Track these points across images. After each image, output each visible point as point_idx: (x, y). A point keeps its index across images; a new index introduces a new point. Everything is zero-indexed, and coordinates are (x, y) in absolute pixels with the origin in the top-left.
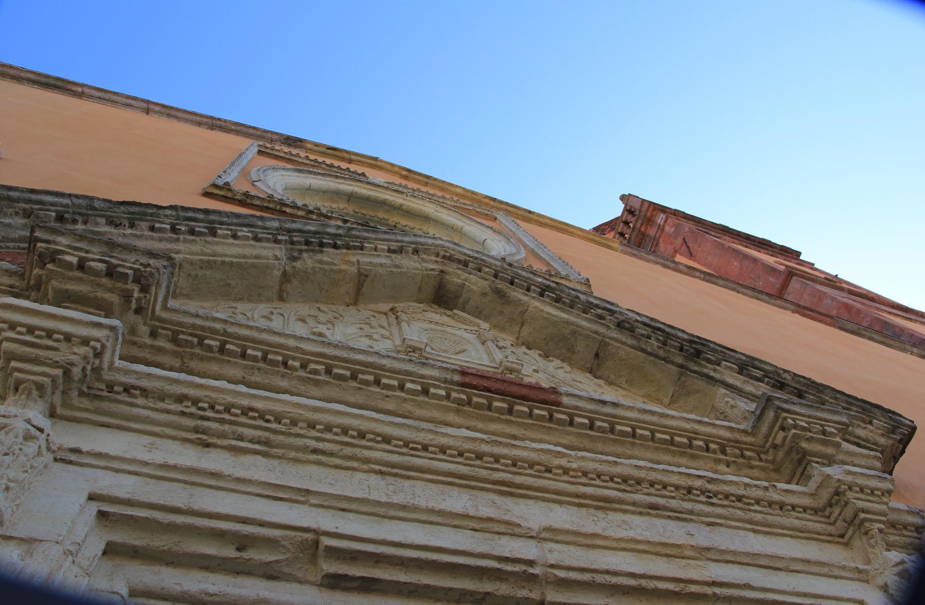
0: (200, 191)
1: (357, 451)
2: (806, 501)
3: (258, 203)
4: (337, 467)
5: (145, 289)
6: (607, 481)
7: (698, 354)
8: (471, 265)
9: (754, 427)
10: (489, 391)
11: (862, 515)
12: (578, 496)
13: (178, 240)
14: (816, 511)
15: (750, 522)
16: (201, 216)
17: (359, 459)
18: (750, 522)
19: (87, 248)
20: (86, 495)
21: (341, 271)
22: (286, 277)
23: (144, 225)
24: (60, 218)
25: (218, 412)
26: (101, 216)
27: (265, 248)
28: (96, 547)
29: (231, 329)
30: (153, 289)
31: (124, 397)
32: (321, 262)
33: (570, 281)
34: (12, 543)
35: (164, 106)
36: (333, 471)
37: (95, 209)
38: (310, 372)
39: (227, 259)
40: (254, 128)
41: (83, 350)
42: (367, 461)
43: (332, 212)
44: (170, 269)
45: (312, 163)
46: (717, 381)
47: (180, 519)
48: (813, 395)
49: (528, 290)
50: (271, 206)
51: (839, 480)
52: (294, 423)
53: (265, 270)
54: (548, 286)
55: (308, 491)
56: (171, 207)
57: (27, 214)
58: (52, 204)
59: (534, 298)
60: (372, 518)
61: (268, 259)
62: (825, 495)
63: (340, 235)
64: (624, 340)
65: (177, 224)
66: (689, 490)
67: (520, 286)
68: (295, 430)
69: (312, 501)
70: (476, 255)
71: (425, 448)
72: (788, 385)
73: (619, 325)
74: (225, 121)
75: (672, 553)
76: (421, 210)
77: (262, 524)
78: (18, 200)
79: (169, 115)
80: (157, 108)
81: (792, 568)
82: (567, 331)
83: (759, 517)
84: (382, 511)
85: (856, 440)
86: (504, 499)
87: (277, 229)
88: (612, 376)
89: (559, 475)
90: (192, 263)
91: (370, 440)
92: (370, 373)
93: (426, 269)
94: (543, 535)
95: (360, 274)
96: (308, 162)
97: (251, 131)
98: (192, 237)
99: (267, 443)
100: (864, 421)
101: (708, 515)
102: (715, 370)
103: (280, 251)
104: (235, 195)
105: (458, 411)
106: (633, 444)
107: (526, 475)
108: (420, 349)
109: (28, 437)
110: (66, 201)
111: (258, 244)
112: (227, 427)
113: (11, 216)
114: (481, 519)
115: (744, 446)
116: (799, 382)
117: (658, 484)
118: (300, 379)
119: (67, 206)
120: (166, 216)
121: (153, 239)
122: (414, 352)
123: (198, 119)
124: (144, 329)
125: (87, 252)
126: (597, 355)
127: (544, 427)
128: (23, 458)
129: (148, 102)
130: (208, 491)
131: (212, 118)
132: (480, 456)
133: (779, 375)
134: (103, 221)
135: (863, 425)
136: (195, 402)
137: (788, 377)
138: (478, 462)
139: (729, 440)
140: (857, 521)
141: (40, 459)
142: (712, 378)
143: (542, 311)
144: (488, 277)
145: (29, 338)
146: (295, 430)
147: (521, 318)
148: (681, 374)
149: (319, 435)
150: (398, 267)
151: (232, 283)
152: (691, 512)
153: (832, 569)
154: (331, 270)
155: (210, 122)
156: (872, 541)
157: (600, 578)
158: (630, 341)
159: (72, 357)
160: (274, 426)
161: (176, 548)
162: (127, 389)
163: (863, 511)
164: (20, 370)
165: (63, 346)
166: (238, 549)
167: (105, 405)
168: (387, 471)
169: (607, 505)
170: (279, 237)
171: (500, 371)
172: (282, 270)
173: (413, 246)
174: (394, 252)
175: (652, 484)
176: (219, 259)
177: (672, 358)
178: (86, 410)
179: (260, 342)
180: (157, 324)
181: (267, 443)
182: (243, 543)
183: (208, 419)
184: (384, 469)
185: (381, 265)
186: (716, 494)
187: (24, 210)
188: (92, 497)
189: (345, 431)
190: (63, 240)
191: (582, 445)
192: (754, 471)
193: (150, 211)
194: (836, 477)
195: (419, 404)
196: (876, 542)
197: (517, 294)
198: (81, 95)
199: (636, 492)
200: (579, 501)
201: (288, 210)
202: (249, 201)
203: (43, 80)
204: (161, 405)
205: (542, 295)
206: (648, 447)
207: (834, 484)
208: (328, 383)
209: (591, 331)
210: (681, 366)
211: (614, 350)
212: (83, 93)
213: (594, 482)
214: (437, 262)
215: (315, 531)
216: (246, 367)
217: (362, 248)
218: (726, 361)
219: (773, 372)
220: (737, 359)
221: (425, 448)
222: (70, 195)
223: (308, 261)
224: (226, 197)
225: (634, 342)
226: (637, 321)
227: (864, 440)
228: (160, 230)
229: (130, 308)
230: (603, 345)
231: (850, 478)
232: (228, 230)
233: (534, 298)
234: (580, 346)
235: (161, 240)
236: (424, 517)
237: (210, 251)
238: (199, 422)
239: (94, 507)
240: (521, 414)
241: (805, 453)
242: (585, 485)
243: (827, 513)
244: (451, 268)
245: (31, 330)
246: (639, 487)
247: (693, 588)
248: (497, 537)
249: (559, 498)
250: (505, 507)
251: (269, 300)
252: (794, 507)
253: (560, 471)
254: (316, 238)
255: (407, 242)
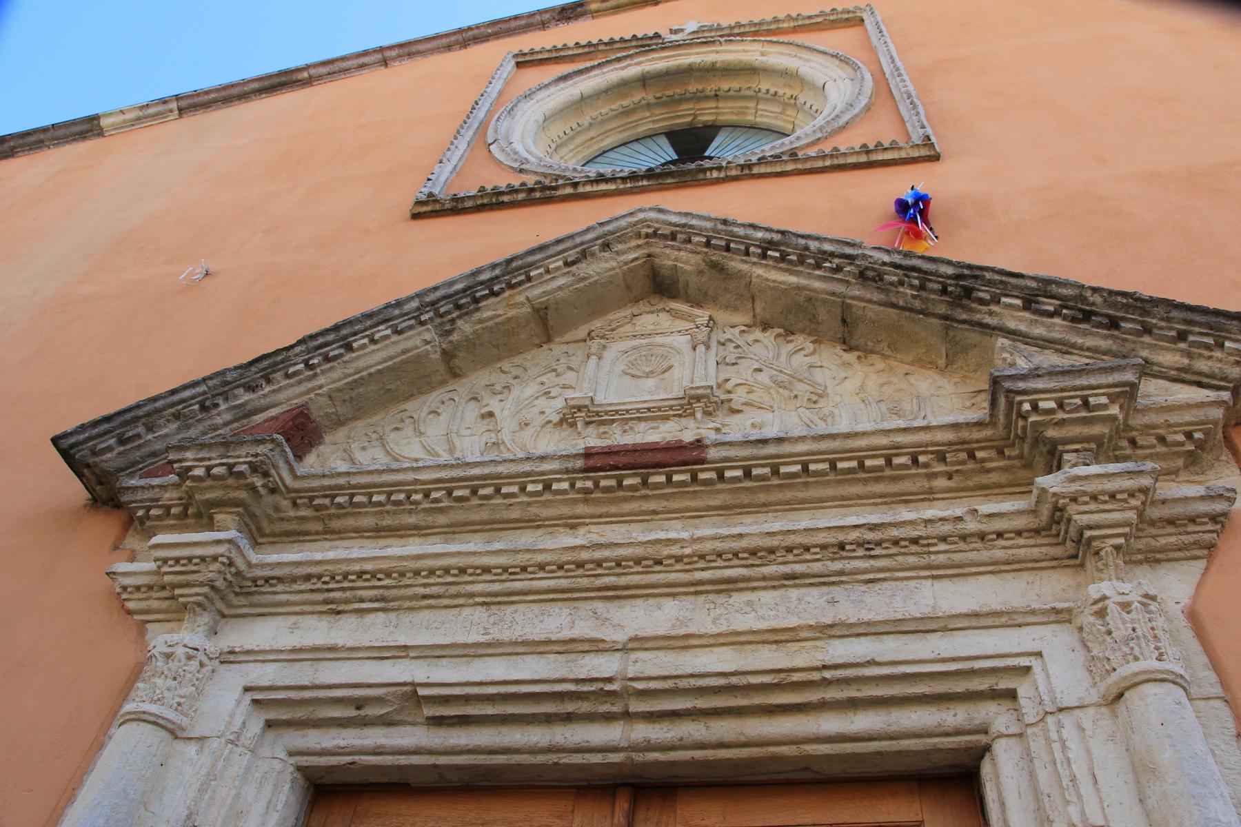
0: (409, 215)
1: (460, 588)
2: (1020, 523)
3: (469, 204)
4: (447, 607)
5: (266, 474)
6: (730, 560)
7: (968, 292)
8: (679, 236)
9: (991, 416)
10: (616, 468)
11: (1088, 533)
12: (693, 584)
13: (315, 375)
14: (1037, 532)
15: (929, 567)
16: (331, 337)
17: (464, 596)
18: (929, 567)
19: (207, 456)
20: (240, 689)
21: (509, 320)
22: (447, 355)
23: (278, 375)
24: (204, 408)
25: (338, 582)
26: (238, 387)
27: (409, 338)
28: (256, 726)
29: (355, 480)
30: (273, 472)
31: (267, 589)
32: (481, 321)
33: (900, 149)
34: (193, 742)
35: (401, 46)
36: (443, 612)
37: (229, 383)
38: (432, 502)
39: (373, 370)
40: (516, 18)
41: (215, 566)
42: (472, 595)
43: (556, 180)
44: (278, 449)
45: (586, 50)
46: (994, 329)
47: (307, 694)
48: (1133, 321)
49: (747, 253)
50: (485, 201)
51: (1055, 494)
52: (402, 574)
53: (421, 359)
54: (771, 242)
55: (406, 647)
56: (300, 342)
57: (177, 416)
58: (193, 398)
59: (754, 263)
60: (464, 659)
61: (417, 348)
62: (1045, 511)
63: (497, 277)
64: (868, 296)
65: (310, 358)
66: (842, 546)
67: (737, 252)
68: (406, 581)
69: (412, 655)
70: (683, 221)
71: (524, 569)
72: (1096, 314)
73: (862, 275)
74: (477, 27)
75: (783, 638)
76: (741, 61)
77: (370, 686)
78: (164, 408)
79: (410, 55)
80: (394, 53)
81: (951, 626)
82: (802, 299)
83: (941, 558)
84: (471, 651)
85: (1196, 378)
86: (609, 605)
87: (418, 309)
88: (870, 344)
89: (671, 565)
90: (339, 390)
91: (471, 575)
92: (489, 485)
93: (626, 264)
94: (630, 646)
95: (536, 311)
96: (580, 51)
97: (514, 24)
98: (328, 366)
99: (383, 599)
100: (1207, 347)
101: (866, 571)
102: (991, 313)
103: (429, 333)
104: (443, 205)
105: (586, 501)
106: (806, 484)
107: (633, 573)
108: (586, 406)
109: (189, 658)
110: (203, 388)
111: (401, 337)
112: (348, 594)
113: (165, 426)
114: (564, 642)
115: (975, 445)
116: (1114, 306)
117: (797, 548)
118: (426, 511)
119: (204, 393)
120: (297, 355)
121: (292, 385)
122: (579, 410)
123: (445, 41)
124: (285, 503)
125: (210, 459)
126: (844, 321)
127: (688, 492)
128: (189, 676)
129: (381, 50)
130: (330, 663)
131: (461, 31)
132: (580, 565)
133: (1084, 299)
134: (242, 390)
135: (1206, 353)
136: (319, 577)
137: (1097, 299)
138: (580, 572)
139: (950, 444)
140: (1083, 541)
141: (204, 670)
142: (987, 326)
143: (767, 280)
144: (699, 249)
145: (177, 569)
146: (406, 581)
147: (747, 294)
148: (947, 328)
149: (426, 581)
150: (584, 279)
151: (392, 387)
152: (841, 573)
153: (1015, 617)
154: (497, 324)
155: (459, 37)
156: (1099, 564)
157: (683, 684)
158: (876, 296)
159: (211, 575)
160: (386, 582)
161: (312, 716)
162: (267, 580)
163: (1090, 528)
164: (182, 596)
165: (202, 567)
166: (358, 708)
167: (256, 598)
168: (491, 601)
169: (731, 586)
170: (423, 318)
171: (685, 401)
172: (439, 350)
173: (600, 241)
174: (573, 263)
175: (789, 550)
176: (365, 373)
177: (931, 308)
178: (244, 606)
179: (382, 485)
180: (294, 495)
181: (383, 599)
182: (359, 703)
183: (332, 590)
184: (488, 600)
185: (560, 288)
186: (879, 543)
187: (173, 414)
188: (247, 689)
189: (447, 571)
190: (189, 455)
191: (738, 501)
192: (991, 475)
193: (279, 358)
194: (1051, 490)
195: (545, 504)
196: (1106, 565)
197: (736, 264)
198: (309, 82)
199: (770, 563)
200: (697, 588)
201: (506, 198)
202: (460, 206)
203: (267, 83)
204: (296, 587)
205: (764, 256)
206: (828, 483)
207: (1051, 500)
208: (451, 508)
209: (827, 293)
210: (945, 318)
211: (860, 312)
212: (310, 77)
213: (713, 564)
214: (638, 246)
215: (413, 684)
216: (376, 513)
217: (529, 279)
218: (1006, 296)
219: (1074, 298)
220: (1022, 289)
221: (524, 569)
222: (204, 380)
223: (465, 327)
224: (436, 211)
225: (882, 297)
226: (884, 264)
227: (1207, 376)
228: (295, 374)
229: (261, 496)
230: (846, 308)
231: (1075, 487)
232: (364, 337)
233: (754, 263)
234: (823, 315)
235: (300, 383)
236: (510, 650)
237: (352, 371)
238: (326, 595)
239: (249, 697)
240: (657, 486)
241: (1054, 443)
242: (703, 569)
243: (1054, 532)
244: (658, 248)
245: (177, 560)
246: (773, 557)
247: (796, 677)
248: (581, 655)
249: (672, 590)
250: (605, 615)
251: (443, 383)
252: (1000, 535)
253: (672, 561)
254: (466, 296)
255: (591, 241)
